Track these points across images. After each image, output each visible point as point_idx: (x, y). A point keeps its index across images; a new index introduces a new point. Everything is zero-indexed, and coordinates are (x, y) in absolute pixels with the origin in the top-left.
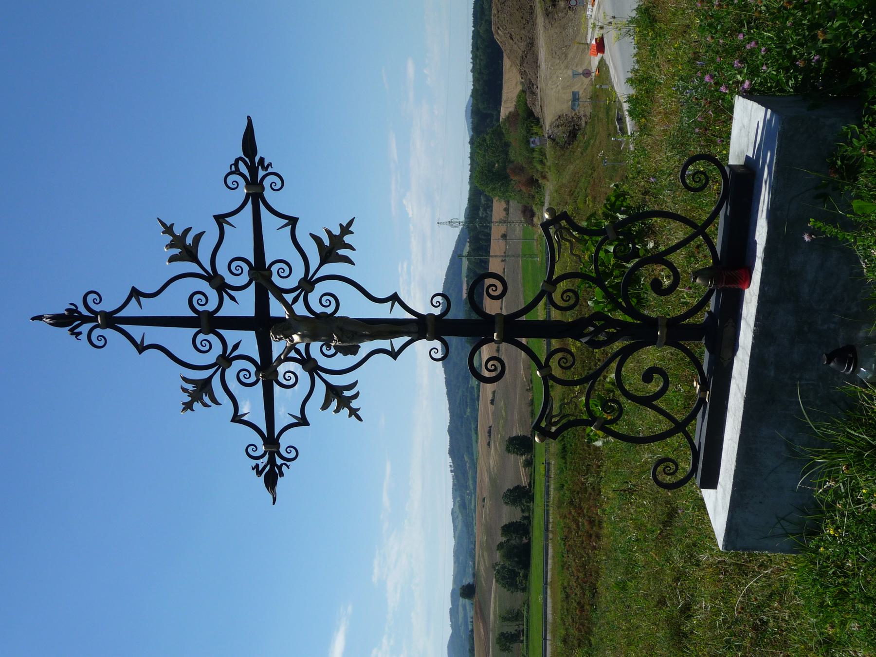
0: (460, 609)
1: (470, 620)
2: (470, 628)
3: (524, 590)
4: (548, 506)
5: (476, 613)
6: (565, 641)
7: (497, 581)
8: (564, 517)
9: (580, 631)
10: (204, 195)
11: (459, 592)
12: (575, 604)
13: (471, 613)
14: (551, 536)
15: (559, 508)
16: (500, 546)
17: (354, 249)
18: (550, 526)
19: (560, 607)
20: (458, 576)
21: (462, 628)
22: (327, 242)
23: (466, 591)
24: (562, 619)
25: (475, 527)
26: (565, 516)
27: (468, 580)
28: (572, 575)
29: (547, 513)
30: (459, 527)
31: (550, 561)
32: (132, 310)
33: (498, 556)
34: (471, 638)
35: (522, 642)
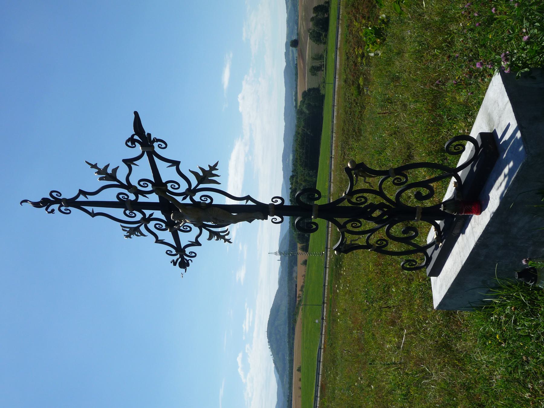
0: (290, 52)
1: (295, 58)
2: (296, 62)
3: (325, 43)
4: (340, 4)
5: (299, 55)
6: (345, 81)
7: (310, 39)
8: (348, 13)
9: (354, 77)
10: (115, 151)
11: (289, 44)
12: (352, 63)
13: (296, 55)
14: (340, 22)
15: (346, 8)
16: (312, 19)
17: (219, 176)
18: (341, 16)
19: (343, 63)
20: (289, 35)
21: (292, 62)
22: (201, 174)
23: (294, 43)
24: (345, 70)
25: (299, 7)
26: (349, 13)
27: (294, 37)
28: (351, 46)
29: (339, 9)
30: (290, 7)
31: (339, 36)
32: (82, 198)
33: (311, 24)
34: (296, 68)
35: (323, 71)
